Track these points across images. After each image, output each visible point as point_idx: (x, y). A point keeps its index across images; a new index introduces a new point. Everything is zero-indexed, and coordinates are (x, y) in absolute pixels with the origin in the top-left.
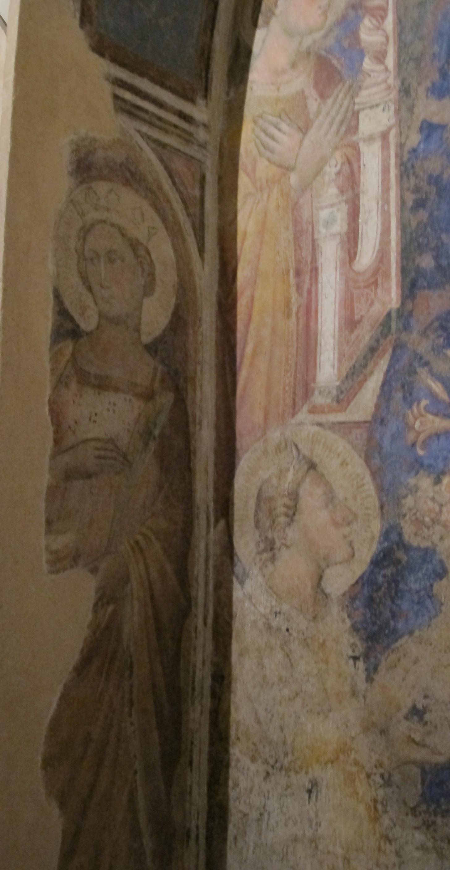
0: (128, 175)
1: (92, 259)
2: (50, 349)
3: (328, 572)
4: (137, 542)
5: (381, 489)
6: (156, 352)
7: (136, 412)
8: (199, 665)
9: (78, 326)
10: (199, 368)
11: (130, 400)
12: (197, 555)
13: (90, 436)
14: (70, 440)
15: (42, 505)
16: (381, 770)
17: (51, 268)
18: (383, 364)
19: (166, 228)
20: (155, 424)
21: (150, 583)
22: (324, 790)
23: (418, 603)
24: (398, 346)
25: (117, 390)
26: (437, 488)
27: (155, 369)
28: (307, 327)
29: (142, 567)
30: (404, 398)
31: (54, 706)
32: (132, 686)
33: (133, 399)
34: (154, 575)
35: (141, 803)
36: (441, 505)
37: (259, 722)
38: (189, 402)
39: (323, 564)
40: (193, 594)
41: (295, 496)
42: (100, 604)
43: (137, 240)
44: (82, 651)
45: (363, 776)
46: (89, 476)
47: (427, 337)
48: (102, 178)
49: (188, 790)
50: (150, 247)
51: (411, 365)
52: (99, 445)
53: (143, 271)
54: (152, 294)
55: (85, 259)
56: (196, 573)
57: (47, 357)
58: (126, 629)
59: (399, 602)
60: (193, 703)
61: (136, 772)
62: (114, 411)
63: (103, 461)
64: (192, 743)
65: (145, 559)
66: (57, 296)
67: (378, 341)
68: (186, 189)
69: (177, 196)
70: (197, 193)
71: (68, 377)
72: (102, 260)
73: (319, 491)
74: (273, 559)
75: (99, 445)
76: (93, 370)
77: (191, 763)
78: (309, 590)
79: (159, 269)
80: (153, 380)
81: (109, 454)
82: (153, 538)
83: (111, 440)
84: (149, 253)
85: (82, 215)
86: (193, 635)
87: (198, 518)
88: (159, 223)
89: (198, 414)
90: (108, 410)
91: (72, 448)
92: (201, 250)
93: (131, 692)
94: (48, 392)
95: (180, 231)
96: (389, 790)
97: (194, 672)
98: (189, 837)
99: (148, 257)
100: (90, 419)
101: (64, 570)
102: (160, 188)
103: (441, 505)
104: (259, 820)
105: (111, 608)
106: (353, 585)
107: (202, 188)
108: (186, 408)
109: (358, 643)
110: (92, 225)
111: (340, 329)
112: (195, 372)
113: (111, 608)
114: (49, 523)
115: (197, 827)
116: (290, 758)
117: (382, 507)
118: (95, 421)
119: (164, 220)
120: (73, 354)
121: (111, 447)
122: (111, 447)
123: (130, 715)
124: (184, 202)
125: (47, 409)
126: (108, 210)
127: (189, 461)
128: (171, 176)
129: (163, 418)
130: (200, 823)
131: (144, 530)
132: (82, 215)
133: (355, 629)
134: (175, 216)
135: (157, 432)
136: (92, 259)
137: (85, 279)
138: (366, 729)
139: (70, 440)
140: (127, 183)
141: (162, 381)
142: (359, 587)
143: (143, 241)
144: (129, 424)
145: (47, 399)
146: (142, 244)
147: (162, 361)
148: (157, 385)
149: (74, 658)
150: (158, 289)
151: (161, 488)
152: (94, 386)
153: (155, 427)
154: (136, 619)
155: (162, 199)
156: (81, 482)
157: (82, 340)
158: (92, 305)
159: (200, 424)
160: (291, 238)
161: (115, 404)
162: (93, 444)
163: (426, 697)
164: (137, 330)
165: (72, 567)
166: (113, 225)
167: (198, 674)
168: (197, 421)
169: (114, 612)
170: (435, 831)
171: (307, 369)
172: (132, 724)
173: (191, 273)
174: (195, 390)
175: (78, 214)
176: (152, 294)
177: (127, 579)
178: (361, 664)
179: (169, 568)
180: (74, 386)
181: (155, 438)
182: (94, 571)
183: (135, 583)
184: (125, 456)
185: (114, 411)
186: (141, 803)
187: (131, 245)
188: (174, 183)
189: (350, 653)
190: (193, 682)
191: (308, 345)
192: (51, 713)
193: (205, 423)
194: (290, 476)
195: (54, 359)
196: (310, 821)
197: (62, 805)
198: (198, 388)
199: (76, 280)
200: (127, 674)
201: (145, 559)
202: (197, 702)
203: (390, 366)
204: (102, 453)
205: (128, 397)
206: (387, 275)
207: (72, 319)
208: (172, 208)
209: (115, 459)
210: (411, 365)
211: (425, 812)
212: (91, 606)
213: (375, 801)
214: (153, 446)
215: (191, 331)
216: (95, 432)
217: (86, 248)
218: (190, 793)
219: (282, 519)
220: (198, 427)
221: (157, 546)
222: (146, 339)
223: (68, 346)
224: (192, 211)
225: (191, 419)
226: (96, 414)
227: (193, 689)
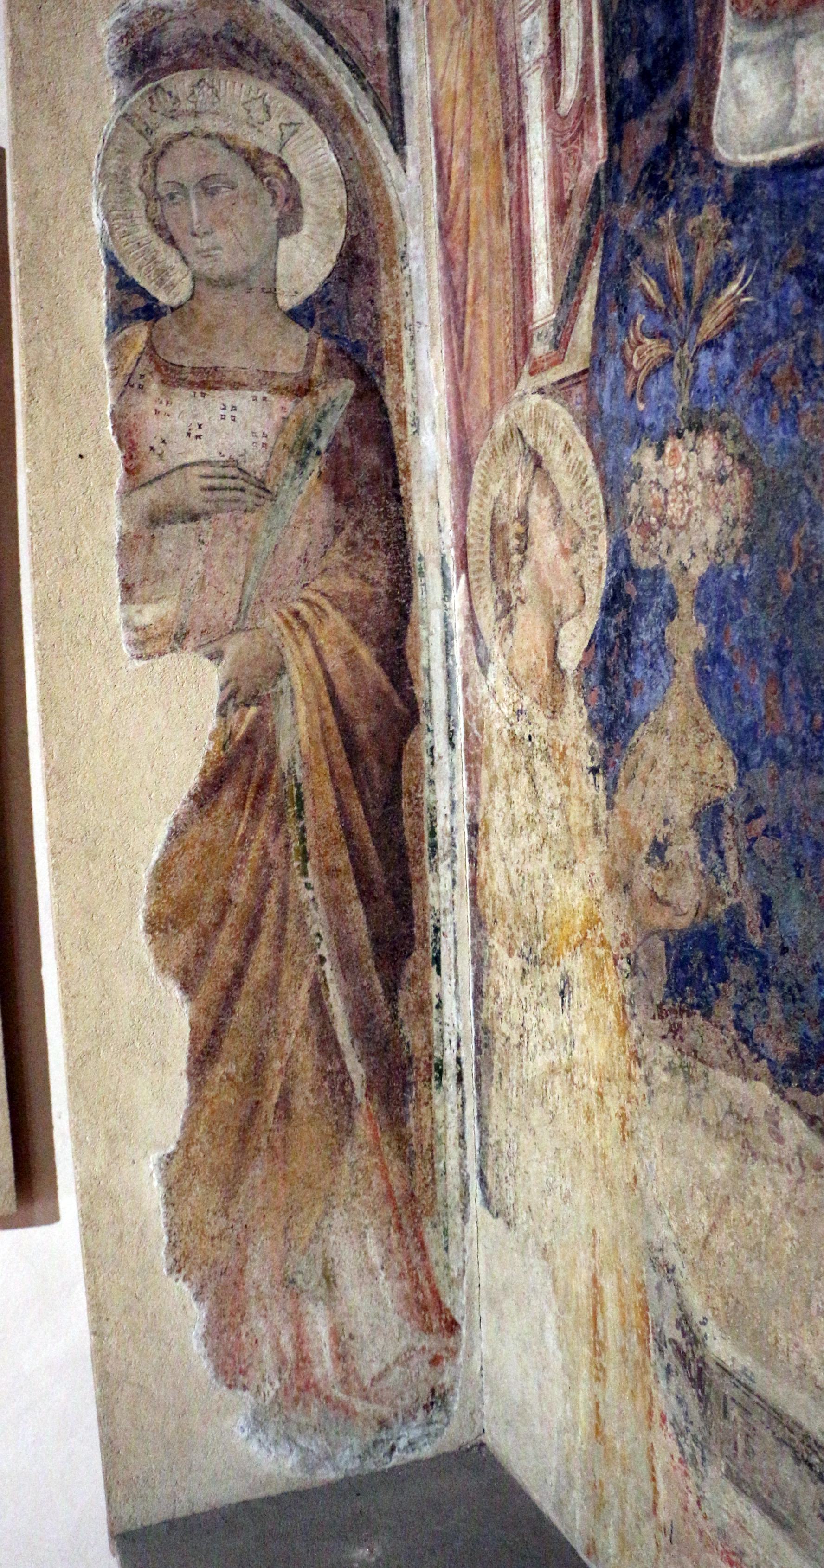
0: (232, 50)
1: (172, 197)
2: (108, 339)
3: (562, 633)
4: (296, 614)
5: (604, 481)
6: (311, 319)
7: (277, 417)
8: (443, 807)
9: (156, 300)
10: (406, 334)
11: (265, 399)
12: (424, 634)
13: (190, 459)
14: (154, 466)
15: (115, 563)
16: (628, 950)
17: (98, 221)
18: (596, 263)
19: (318, 120)
20: (319, 432)
21: (327, 675)
22: (575, 990)
23: (651, 665)
24: (609, 231)
25: (237, 386)
26: (660, 463)
27: (311, 345)
28: (520, 230)
29: (309, 652)
30: (620, 317)
31: (159, 846)
32: (303, 830)
33: (271, 398)
34: (335, 663)
35: (337, 1006)
36: (666, 491)
37: (512, 892)
38: (388, 392)
39: (556, 622)
40: (421, 694)
41: (524, 517)
42: (230, 704)
43: (259, 151)
44: (204, 771)
45: (610, 961)
46: (195, 518)
47: (637, 205)
48: (179, 66)
49: (435, 1001)
50: (286, 158)
51: (623, 257)
52: (209, 470)
53: (274, 195)
54: (298, 231)
55: (159, 199)
56: (424, 662)
57: (103, 351)
58: (285, 746)
59: (632, 668)
60: (434, 868)
61: (322, 960)
62: (233, 419)
63: (218, 494)
64: (437, 930)
65: (313, 639)
66: (112, 262)
67: (588, 229)
68: (357, 44)
69: (339, 62)
70: (383, 46)
71: (142, 376)
72: (192, 192)
73: (546, 502)
74: (511, 626)
75: (209, 470)
76: (187, 361)
77: (437, 960)
78: (546, 670)
79: (306, 186)
80: (308, 363)
81: (231, 483)
82: (328, 608)
83: (232, 463)
84: (285, 167)
85: (147, 132)
86: (427, 760)
87: (422, 574)
88: (301, 114)
89: (410, 408)
90: (223, 417)
91: (159, 478)
92: (398, 141)
93: (303, 840)
94: (109, 403)
95: (349, 119)
96: (636, 979)
97: (433, 819)
98: (441, 1072)
99: (283, 173)
100: (189, 434)
101: (161, 654)
102: (301, 55)
103: (666, 491)
104: (520, 1045)
105: (253, 711)
106: (587, 650)
107: (394, 36)
108: (382, 402)
109: (597, 745)
110: (168, 145)
111: (552, 223)
112: (398, 341)
113: (253, 711)
114: (127, 588)
115: (459, 1061)
116: (543, 944)
117: (607, 512)
118: (198, 437)
119: (312, 107)
120: (150, 342)
121: (234, 472)
122: (234, 472)
123: (305, 873)
124: (353, 67)
125: (109, 427)
126: (196, 114)
127: (396, 484)
128: (322, 31)
129: (334, 421)
130: (463, 1055)
131: (308, 594)
132: (147, 132)
133: (593, 723)
134: (337, 97)
135: (323, 444)
136: (172, 197)
137: (160, 228)
138: (610, 886)
139: (154, 466)
140: (232, 63)
141: (328, 363)
142: (592, 650)
143: (273, 149)
144: (265, 436)
145: (108, 413)
146: (269, 155)
147: (326, 333)
148: (316, 371)
149: (192, 781)
150: (309, 217)
151: (338, 530)
152: (192, 384)
153: (318, 437)
154: (303, 728)
155: (305, 74)
156: (181, 526)
157: (164, 321)
158: (180, 265)
159: (416, 424)
160: (497, 84)
161: (234, 408)
162: (196, 470)
163: (666, 822)
164: (273, 292)
165: (173, 650)
166: (208, 136)
167: (442, 825)
168: (409, 419)
169: (260, 717)
170: (682, 1039)
171: (524, 305)
172: (308, 886)
173: (378, 183)
174: (400, 371)
175: (140, 132)
176: (297, 227)
177: (281, 670)
178: (600, 779)
179: (366, 654)
180: (154, 387)
181: (319, 453)
182: (216, 656)
183: (295, 675)
184: (261, 485)
185: (233, 419)
186: (337, 1006)
187: (247, 160)
188: (330, 42)
189: (590, 764)
190: (433, 834)
191: (522, 262)
192: (155, 856)
193: (426, 421)
194: (518, 486)
195: (116, 352)
196: (565, 1039)
197: (188, 987)
198: (407, 367)
199: (144, 231)
200: (292, 811)
201: (313, 639)
202: (442, 867)
203: (603, 268)
204: (216, 482)
205: (260, 394)
206: (592, 110)
207: (144, 293)
208: (327, 84)
209: (242, 490)
210: (623, 257)
211: (673, 1011)
212: (214, 707)
213: (623, 998)
214: (315, 465)
215: (384, 276)
216: (199, 451)
217: (160, 180)
218: (439, 1006)
219: (516, 558)
220: (411, 430)
221: (337, 620)
222: (287, 302)
223: (140, 333)
224: (371, 79)
225: (394, 418)
226: (200, 426)
227: (434, 846)
